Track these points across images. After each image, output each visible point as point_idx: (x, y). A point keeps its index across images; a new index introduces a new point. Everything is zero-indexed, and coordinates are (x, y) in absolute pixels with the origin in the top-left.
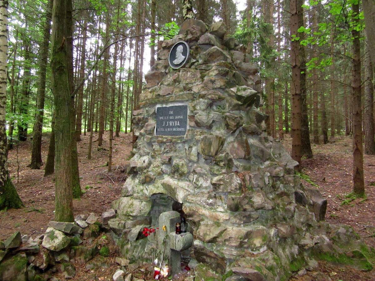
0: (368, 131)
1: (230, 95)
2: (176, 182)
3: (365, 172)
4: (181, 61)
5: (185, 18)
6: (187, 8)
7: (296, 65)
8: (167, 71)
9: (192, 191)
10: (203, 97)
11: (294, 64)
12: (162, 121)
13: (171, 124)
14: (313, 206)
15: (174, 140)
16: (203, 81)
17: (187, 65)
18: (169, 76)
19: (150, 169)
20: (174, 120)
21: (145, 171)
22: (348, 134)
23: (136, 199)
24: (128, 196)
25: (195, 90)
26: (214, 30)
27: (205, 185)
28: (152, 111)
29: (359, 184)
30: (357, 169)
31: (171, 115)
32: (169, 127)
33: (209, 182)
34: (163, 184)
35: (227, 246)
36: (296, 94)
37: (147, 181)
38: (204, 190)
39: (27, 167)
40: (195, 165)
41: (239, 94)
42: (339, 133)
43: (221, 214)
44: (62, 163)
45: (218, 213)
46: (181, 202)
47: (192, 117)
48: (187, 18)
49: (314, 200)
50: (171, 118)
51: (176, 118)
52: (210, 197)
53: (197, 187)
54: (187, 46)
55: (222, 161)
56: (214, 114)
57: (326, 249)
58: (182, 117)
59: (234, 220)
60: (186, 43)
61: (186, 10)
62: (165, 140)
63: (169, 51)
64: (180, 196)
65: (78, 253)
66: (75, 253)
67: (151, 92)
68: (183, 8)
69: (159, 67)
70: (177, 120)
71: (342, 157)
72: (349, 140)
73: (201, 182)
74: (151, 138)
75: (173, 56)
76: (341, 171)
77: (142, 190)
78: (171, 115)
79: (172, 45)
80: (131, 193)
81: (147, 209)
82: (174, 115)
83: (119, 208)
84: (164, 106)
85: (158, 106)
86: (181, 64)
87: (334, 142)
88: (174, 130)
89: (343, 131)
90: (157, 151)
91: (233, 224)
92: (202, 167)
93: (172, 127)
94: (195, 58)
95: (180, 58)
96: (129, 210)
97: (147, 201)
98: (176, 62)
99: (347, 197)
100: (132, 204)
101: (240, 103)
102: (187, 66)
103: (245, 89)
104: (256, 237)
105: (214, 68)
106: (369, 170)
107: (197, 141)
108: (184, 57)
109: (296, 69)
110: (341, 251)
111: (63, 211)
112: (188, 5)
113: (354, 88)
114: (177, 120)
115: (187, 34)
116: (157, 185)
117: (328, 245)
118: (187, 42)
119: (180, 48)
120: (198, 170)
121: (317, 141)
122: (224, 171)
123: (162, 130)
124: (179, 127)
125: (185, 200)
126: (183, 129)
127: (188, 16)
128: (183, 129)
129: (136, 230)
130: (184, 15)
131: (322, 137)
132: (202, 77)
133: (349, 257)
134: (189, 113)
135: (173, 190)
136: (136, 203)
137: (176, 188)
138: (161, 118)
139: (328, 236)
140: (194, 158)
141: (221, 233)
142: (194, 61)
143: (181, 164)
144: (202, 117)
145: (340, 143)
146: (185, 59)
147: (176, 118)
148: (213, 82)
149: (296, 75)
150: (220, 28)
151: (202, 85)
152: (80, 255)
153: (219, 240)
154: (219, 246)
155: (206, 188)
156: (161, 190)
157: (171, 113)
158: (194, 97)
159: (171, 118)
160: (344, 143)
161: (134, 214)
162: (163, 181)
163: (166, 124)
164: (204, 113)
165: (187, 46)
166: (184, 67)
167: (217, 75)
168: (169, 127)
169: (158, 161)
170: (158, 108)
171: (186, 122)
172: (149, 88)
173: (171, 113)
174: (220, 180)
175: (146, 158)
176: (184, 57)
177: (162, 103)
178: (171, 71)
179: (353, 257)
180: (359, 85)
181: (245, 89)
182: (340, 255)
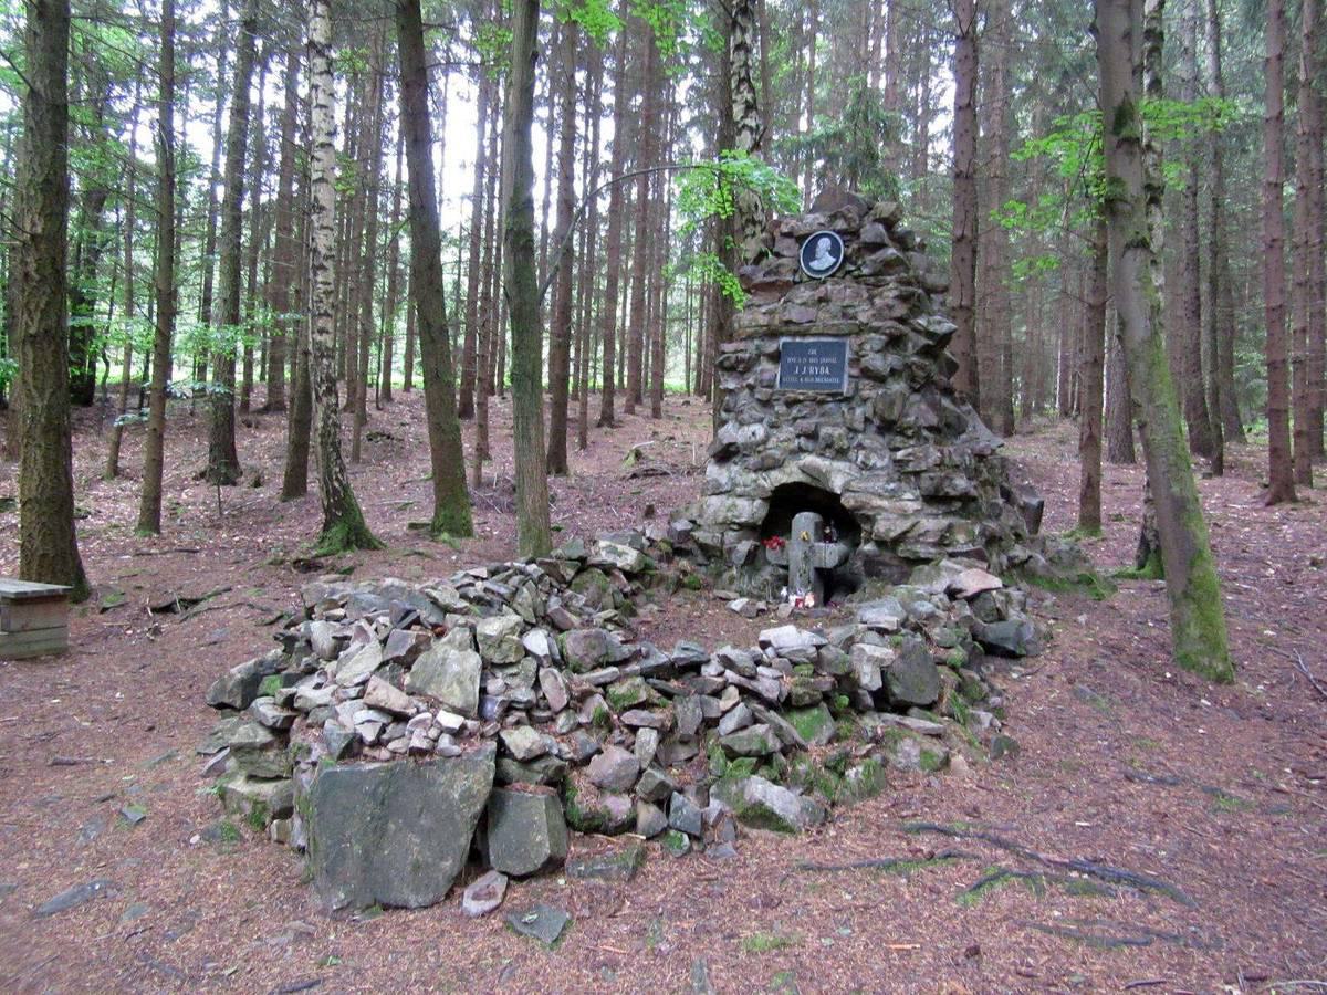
0: (1117, 405)
1: (915, 330)
2: (827, 463)
3: (1104, 496)
4: (827, 265)
6: (747, 101)
7: (963, 237)
8: (797, 279)
9: (858, 475)
10: (876, 330)
11: (959, 233)
12: (793, 366)
13: (811, 372)
14: (1024, 508)
15: (820, 397)
16: (872, 304)
17: (839, 272)
18: (802, 289)
19: (770, 445)
21: (761, 448)
22: (1065, 413)
23: (740, 496)
24: (721, 493)
25: (863, 318)
27: (879, 464)
28: (771, 347)
29: (1091, 508)
30: (1089, 478)
33: (886, 460)
34: (803, 470)
35: (923, 543)
36: (961, 307)
37: (764, 468)
38: (880, 472)
39: (195, 478)
40: (860, 436)
41: (931, 329)
42: (1040, 410)
43: (910, 503)
44: (533, 442)
45: (903, 503)
46: (839, 492)
48: (744, 126)
49: (1027, 500)
51: (824, 360)
52: (890, 480)
53: (865, 466)
55: (910, 428)
56: (893, 359)
57: (1040, 572)
58: (834, 361)
60: (838, 237)
61: (743, 106)
62: (801, 397)
64: (837, 484)
65: (655, 580)
66: (651, 583)
68: (735, 101)
69: (783, 270)
70: (825, 365)
71: (1055, 465)
72: (1071, 430)
74: (772, 394)
75: (810, 254)
76: (1052, 495)
77: (755, 481)
78: (814, 356)
79: (808, 235)
80: (726, 488)
82: (819, 355)
83: (700, 516)
86: (828, 269)
87: (1032, 433)
88: (818, 380)
89: (1053, 408)
91: (928, 515)
92: (870, 439)
94: (854, 263)
95: (824, 260)
96: (729, 514)
97: (763, 499)
98: (815, 265)
99: (1065, 536)
100: (734, 505)
101: (931, 342)
102: (839, 274)
103: (939, 322)
104: (959, 532)
105: (891, 285)
106: (1112, 492)
107: (865, 401)
108: (834, 260)
109: (963, 244)
110: (1062, 575)
111: (539, 539)
112: (749, 97)
113: (1091, 307)
115: (834, 217)
117: (1044, 567)
118: (839, 232)
119: (824, 243)
120: (867, 442)
122: (912, 442)
123: (794, 380)
125: (846, 489)
129: (744, 547)
132: (871, 299)
133: (1073, 583)
135: (825, 475)
136: (742, 503)
137: (828, 472)
139: (1044, 556)
141: (913, 526)
142: (853, 268)
143: (836, 433)
144: (878, 363)
145: (1048, 435)
146: (835, 264)
148: (890, 308)
149: (963, 260)
151: (871, 312)
152: (658, 585)
153: (909, 535)
155: (882, 468)
156: (798, 477)
157: (814, 352)
158: (861, 329)
159: (812, 360)
160: (1057, 436)
161: (743, 520)
164: (879, 356)
166: (832, 276)
167: (896, 297)
170: (784, 344)
171: (843, 370)
172: (759, 306)
173: (814, 352)
174: (910, 454)
176: (834, 260)
177: (795, 334)
178: (805, 279)
179: (1079, 582)
180: (1101, 300)
181: (939, 322)
182: (1061, 580)
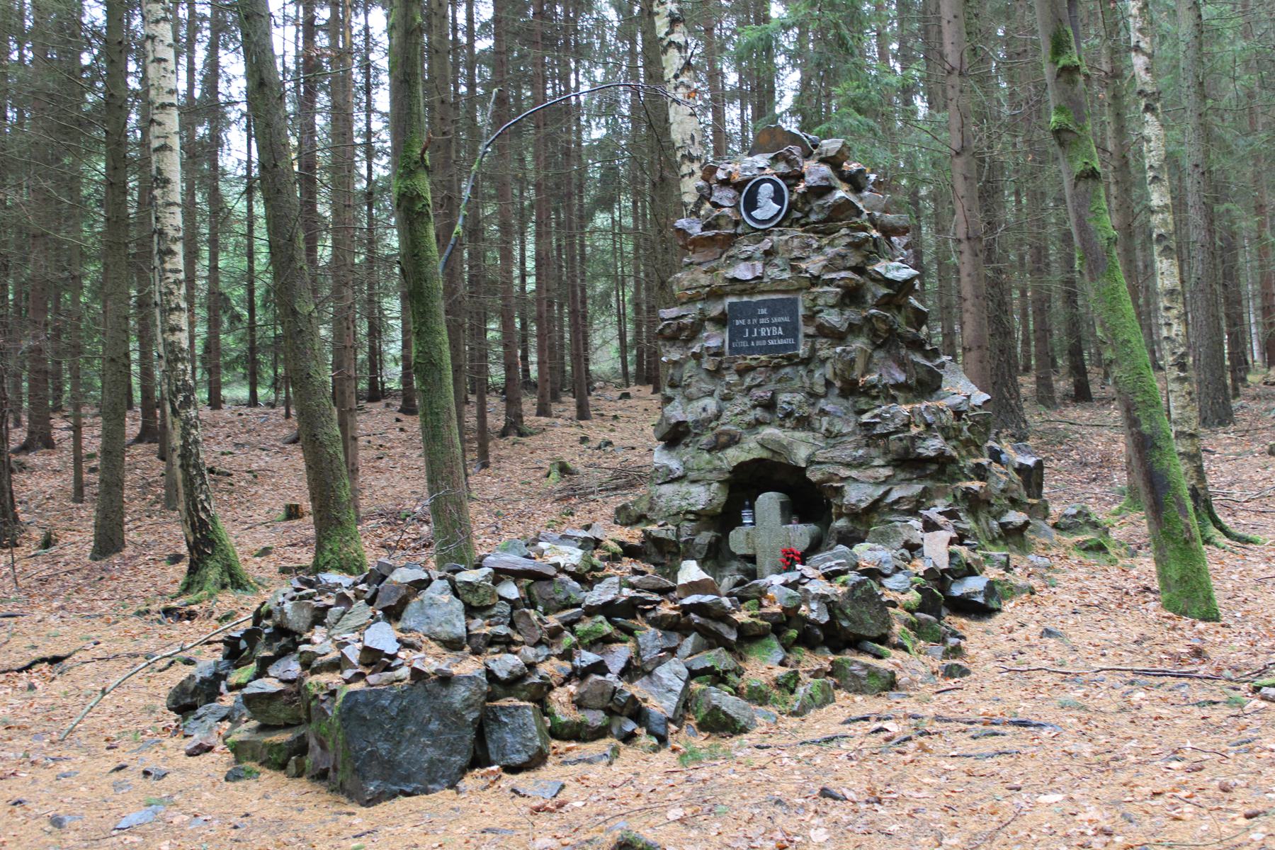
5: (665, 43)
13: (763, 334)
20: (770, 325)
21: (713, 424)
26: (830, 154)
31: (764, 316)
32: (759, 338)
40: (822, 400)
47: (810, 318)
50: (762, 321)
51: (775, 320)
54: (784, 186)
56: (852, 314)
58: (787, 319)
59: (901, 476)
60: (780, 181)
63: (741, 193)
67: (706, 272)
70: (777, 325)
73: (839, 426)
75: (752, 204)
78: (764, 316)
81: (722, 498)
84: (745, 299)
85: (734, 299)
88: (772, 342)
90: (735, 385)
93: (767, 338)
101: (891, 291)
114: (777, 325)
116: (746, 447)
121: (1045, 396)
124: (780, 337)
126: (790, 341)
127: (675, 38)
128: (790, 341)
130: (662, 35)
131: (1063, 385)
134: (801, 311)
138: (738, 322)
140: (820, 389)
144: (832, 318)
146: (780, 211)
147: (775, 320)
150: (838, 152)
154: (884, 514)
159: (762, 321)
162: (759, 437)
163: (751, 332)
165: (784, 186)
168: (759, 338)
169: (742, 402)
170: (731, 304)
173: (764, 311)
175: (711, 404)
